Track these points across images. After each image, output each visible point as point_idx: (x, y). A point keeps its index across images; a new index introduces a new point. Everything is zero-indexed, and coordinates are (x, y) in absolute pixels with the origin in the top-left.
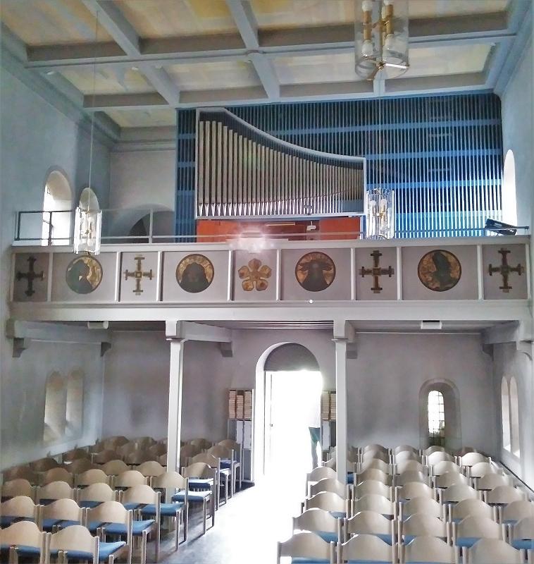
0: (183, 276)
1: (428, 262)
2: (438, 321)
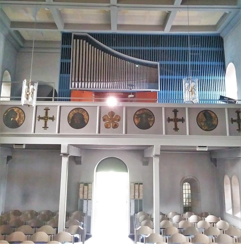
0: (71, 120)
1: (202, 116)
2: (206, 147)
